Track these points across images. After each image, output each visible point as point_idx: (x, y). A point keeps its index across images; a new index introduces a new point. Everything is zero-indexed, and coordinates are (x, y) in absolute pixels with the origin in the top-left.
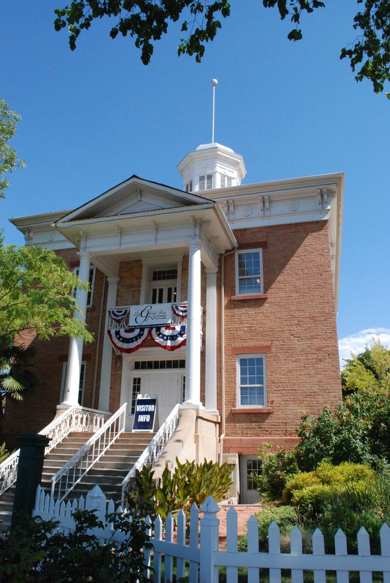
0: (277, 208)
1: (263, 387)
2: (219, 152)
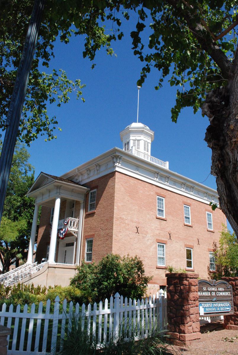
0: (103, 168)
1: (92, 253)
2: (130, 129)
